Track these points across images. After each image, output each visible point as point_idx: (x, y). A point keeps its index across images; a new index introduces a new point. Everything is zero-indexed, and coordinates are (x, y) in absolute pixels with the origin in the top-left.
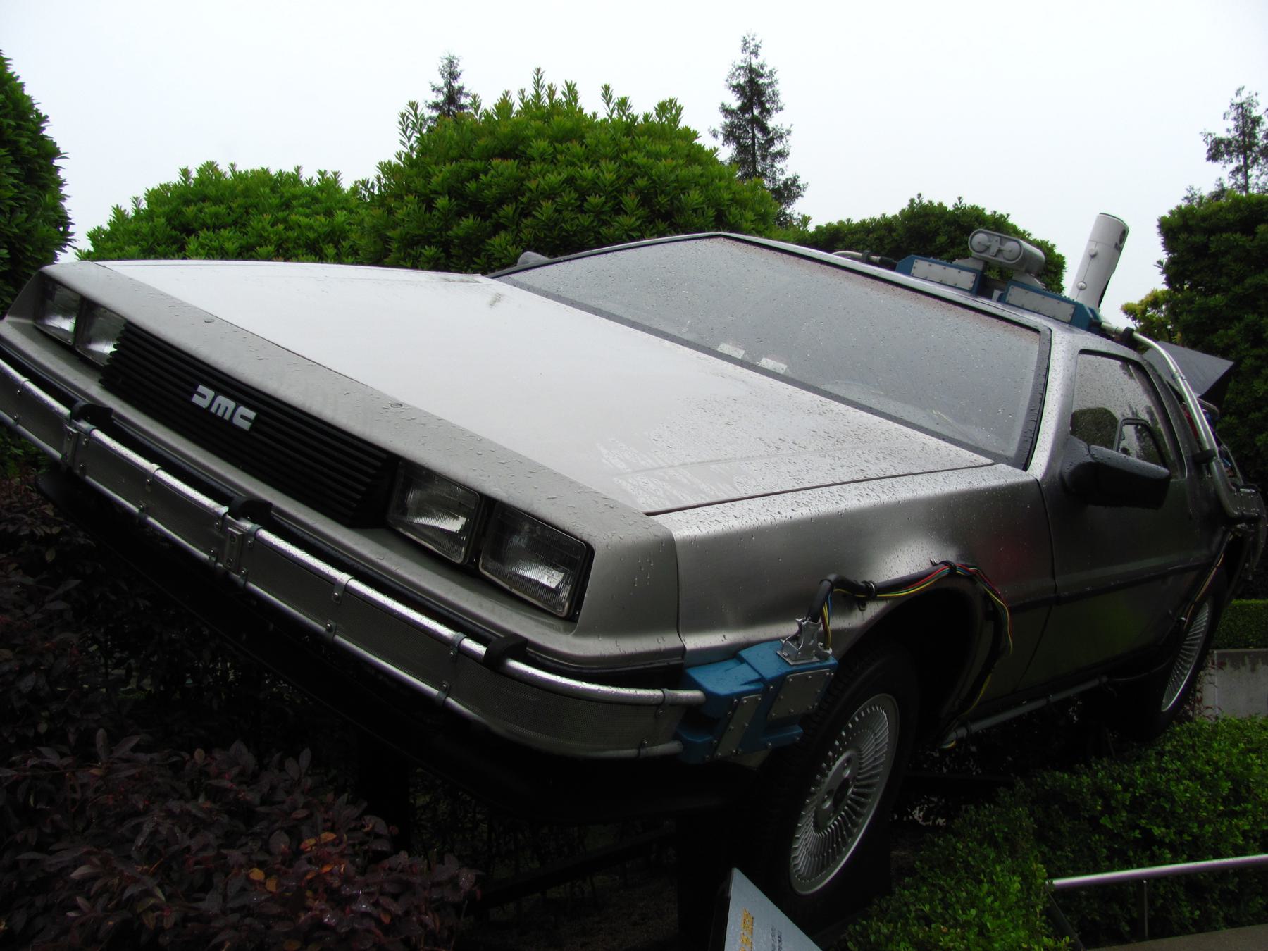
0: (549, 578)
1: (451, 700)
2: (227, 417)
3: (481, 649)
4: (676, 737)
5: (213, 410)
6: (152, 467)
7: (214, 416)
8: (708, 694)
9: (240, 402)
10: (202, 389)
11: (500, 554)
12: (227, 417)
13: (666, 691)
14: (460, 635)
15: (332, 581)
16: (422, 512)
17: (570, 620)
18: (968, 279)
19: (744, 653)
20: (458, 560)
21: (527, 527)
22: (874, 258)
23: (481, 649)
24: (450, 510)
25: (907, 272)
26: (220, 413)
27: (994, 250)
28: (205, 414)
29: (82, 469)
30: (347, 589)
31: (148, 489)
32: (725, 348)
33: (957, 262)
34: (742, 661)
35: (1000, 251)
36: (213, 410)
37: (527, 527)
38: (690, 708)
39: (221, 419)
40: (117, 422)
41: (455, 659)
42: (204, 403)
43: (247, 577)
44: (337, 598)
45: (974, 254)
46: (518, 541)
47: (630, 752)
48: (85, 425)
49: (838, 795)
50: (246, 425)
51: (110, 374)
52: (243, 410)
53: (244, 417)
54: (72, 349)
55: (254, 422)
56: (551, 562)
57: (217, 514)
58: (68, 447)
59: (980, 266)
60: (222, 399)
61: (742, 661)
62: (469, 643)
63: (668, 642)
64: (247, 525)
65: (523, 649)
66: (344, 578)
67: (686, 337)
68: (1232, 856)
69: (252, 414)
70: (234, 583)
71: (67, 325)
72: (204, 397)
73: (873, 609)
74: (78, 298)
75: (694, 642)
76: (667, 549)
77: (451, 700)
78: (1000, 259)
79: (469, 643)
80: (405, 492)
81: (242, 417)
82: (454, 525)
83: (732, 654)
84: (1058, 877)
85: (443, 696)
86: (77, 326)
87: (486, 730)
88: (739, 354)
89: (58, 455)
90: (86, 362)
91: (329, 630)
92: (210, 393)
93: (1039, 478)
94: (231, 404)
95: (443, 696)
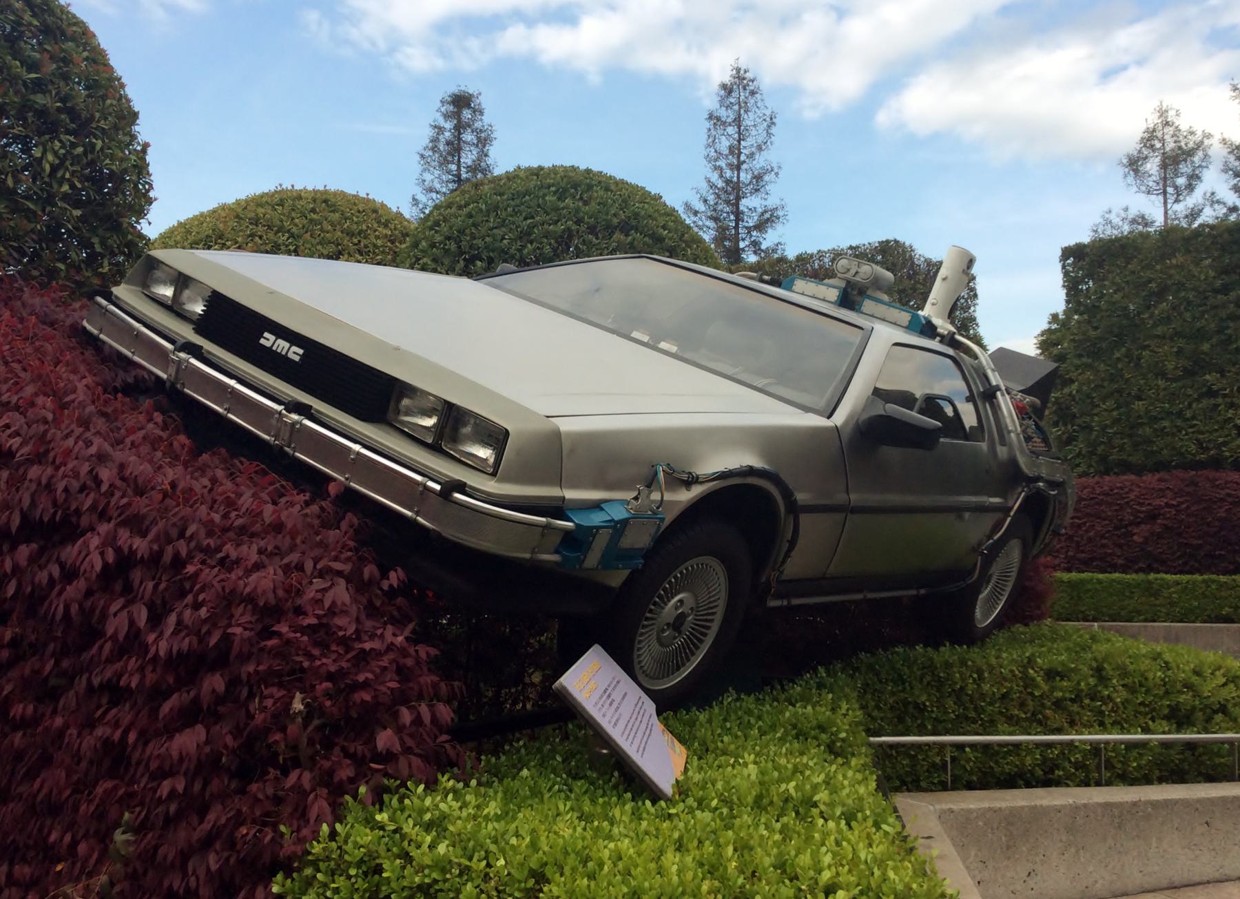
0: (484, 453)
1: (419, 518)
2: (284, 353)
3: (438, 487)
4: (557, 552)
5: (274, 348)
6: (232, 383)
7: (275, 352)
8: (577, 525)
9: (292, 343)
10: (266, 335)
11: (455, 439)
12: (284, 353)
13: (550, 519)
14: (426, 479)
15: (349, 449)
16: (407, 414)
17: (494, 472)
18: (833, 294)
19: (603, 505)
20: (430, 441)
21: (472, 421)
22: (766, 277)
23: (438, 487)
24: (427, 413)
25: (789, 289)
26: (279, 351)
27: (853, 271)
28: (269, 350)
29: (183, 384)
30: (358, 453)
31: (229, 396)
32: (635, 334)
33: (826, 281)
34: (602, 509)
35: (857, 273)
36: (274, 348)
37: (472, 421)
38: (567, 533)
39: (280, 354)
40: (206, 355)
41: (422, 493)
42: (268, 344)
43: (294, 450)
44: (352, 459)
45: (839, 275)
46: (467, 430)
47: (527, 556)
48: (183, 355)
49: (677, 624)
50: (297, 358)
51: (202, 325)
52: (294, 349)
53: (295, 353)
54: (174, 308)
55: (302, 356)
56: (485, 443)
57: (276, 411)
58: (172, 370)
59: (843, 284)
60: (280, 341)
61: (602, 509)
62: (431, 484)
63: (554, 492)
64: (295, 417)
65: (461, 487)
66: (357, 447)
67: (610, 326)
68: (849, 602)
69: (301, 351)
70: (287, 454)
71: (167, 292)
72: (268, 340)
73: (697, 491)
74: (176, 274)
75: (571, 494)
76: (557, 435)
77: (419, 518)
78: (857, 279)
79: (431, 484)
80: (399, 401)
81: (294, 353)
82: (429, 422)
83: (597, 506)
84: (872, 736)
85: (414, 516)
86: (175, 294)
87: (439, 534)
88: (646, 339)
89: (164, 376)
90: (182, 316)
91: (347, 479)
92: (272, 338)
93: (838, 425)
94: (287, 345)
95: (414, 516)
